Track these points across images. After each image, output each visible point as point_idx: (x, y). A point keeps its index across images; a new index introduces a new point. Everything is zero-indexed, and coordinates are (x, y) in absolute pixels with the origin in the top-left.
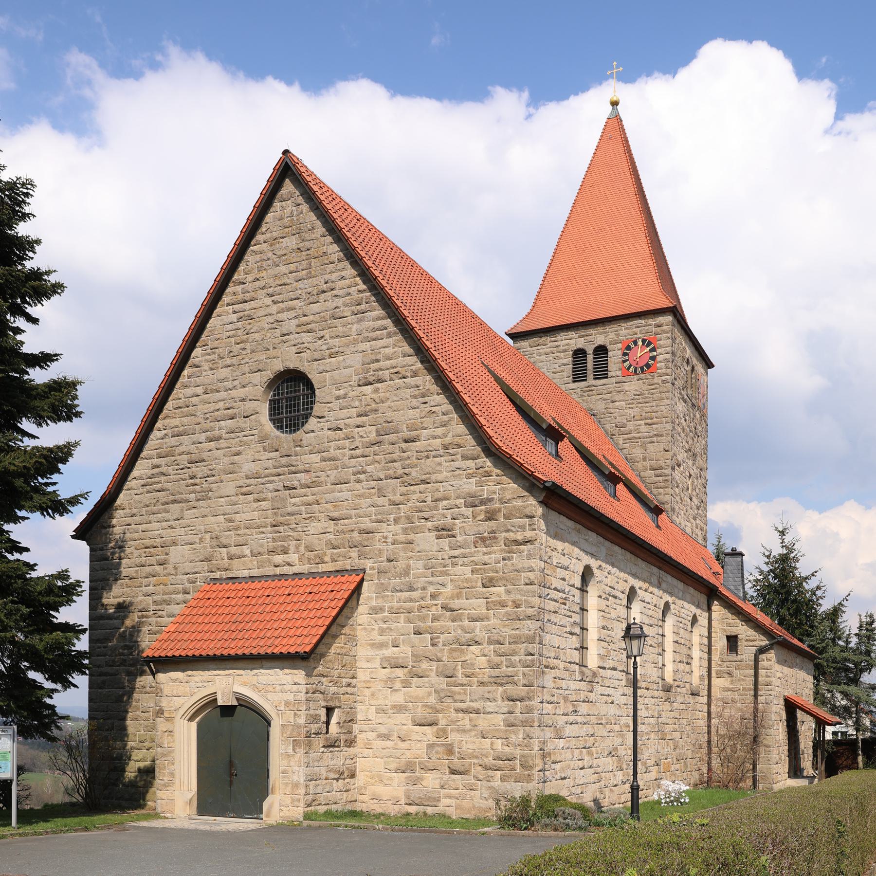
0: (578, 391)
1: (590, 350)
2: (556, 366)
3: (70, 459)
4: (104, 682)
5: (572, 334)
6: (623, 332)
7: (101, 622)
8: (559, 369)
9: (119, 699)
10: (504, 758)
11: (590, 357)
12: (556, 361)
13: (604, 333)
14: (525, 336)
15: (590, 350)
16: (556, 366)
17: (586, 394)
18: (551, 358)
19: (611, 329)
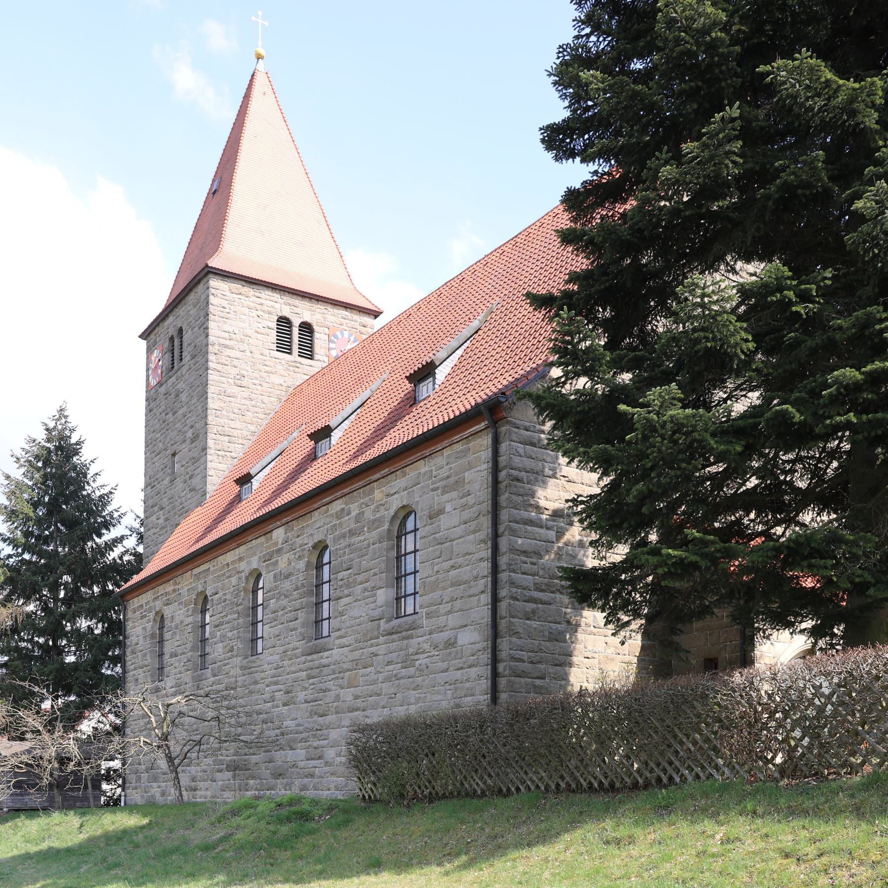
0: (283, 362)
1: (296, 322)
2: (260, 326)
3: (550, 155)
4: (534, 612)
5: (276, 296)
6: (330, 318)
7: (529, 528)
8: (262, 330)
9: (557, 638)
10: (535, 675)
11: (296, 331)
12: (259, 320)
13: (311, 310)
14: (228, 277)
15: (296, 322)
16: (260, 326)
17: (291, 368)
18: (254, 315)
19: (320, 308)
